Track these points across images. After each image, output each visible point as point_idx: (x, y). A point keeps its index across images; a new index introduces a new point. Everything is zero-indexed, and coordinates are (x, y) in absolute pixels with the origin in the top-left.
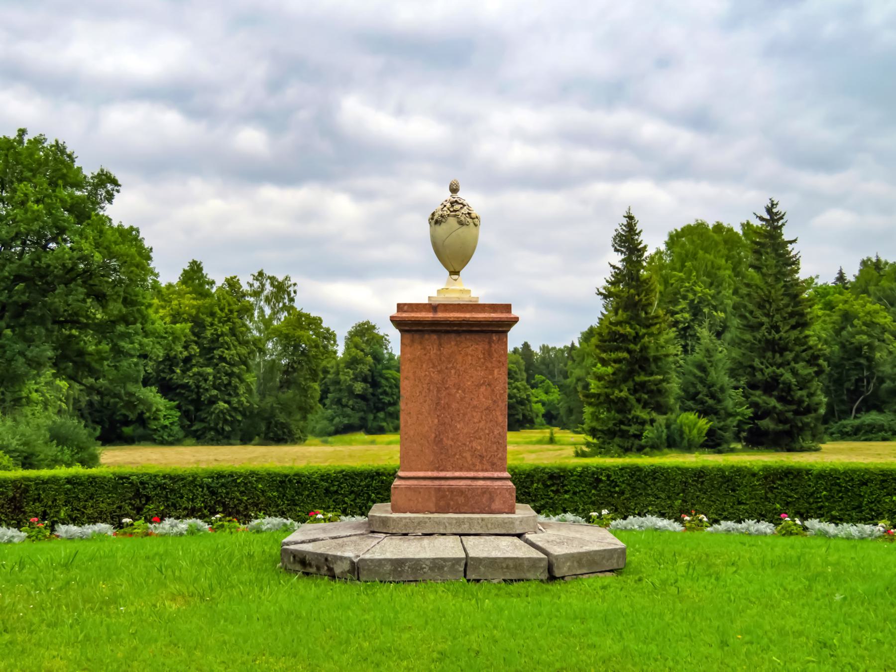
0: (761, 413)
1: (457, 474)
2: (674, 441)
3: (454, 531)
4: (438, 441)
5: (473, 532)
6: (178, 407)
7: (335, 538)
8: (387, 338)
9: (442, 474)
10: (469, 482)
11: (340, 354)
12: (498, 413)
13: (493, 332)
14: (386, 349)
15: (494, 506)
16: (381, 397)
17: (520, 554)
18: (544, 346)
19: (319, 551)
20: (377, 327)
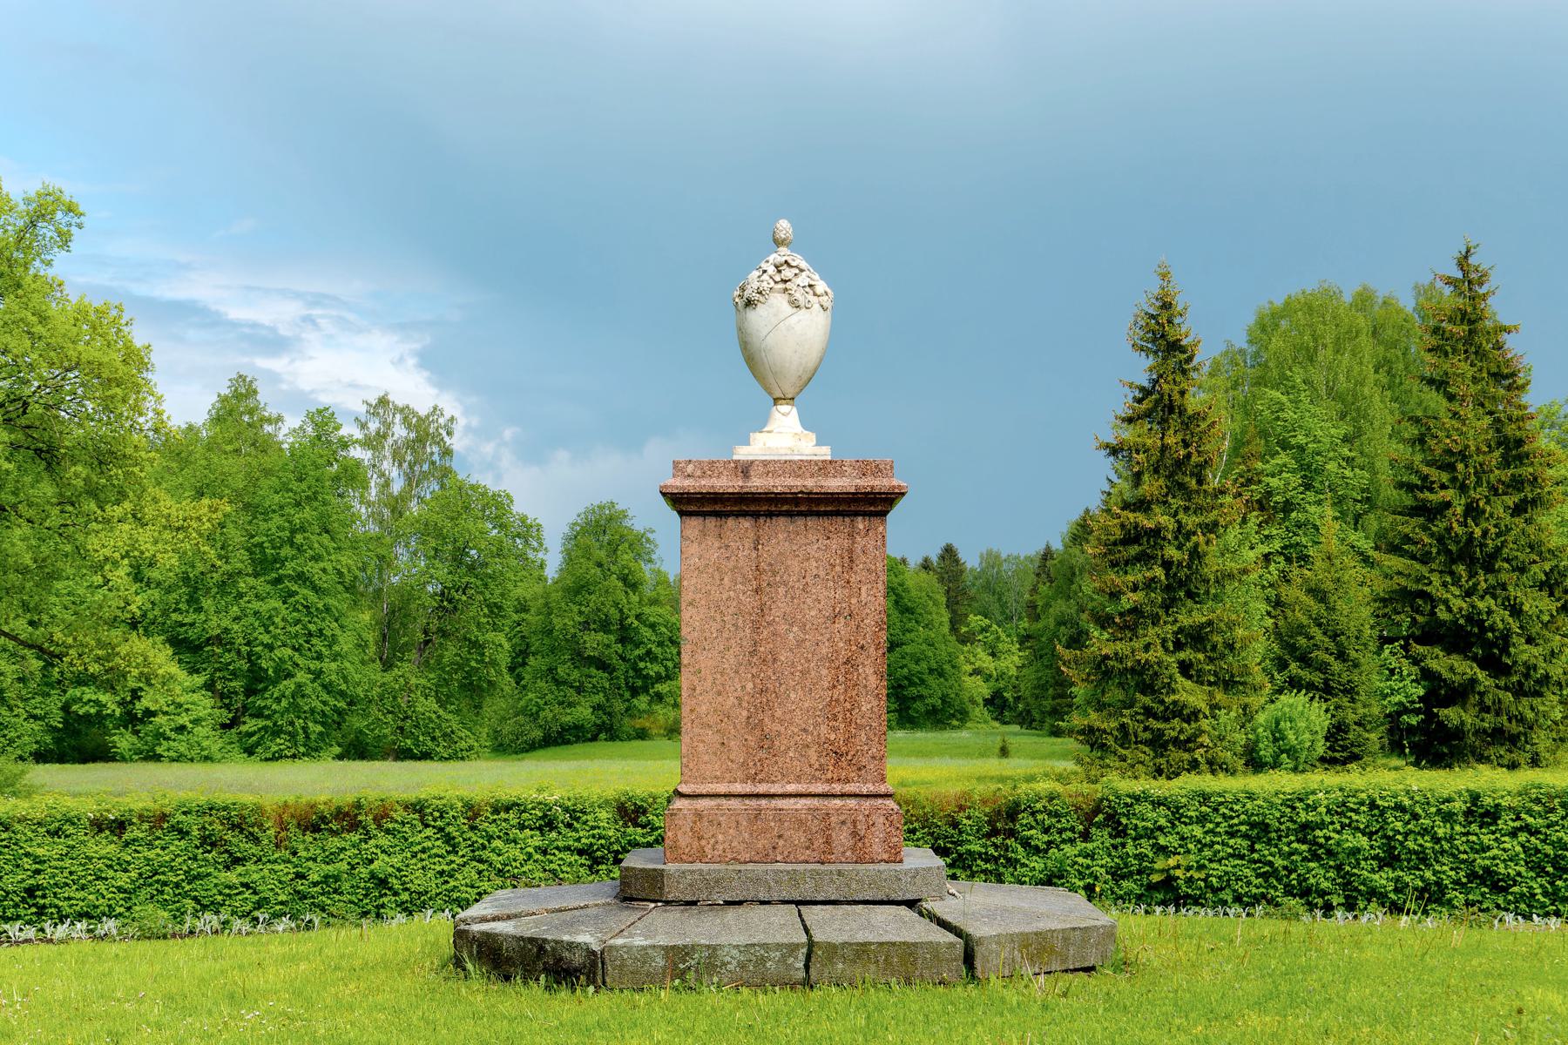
0: (1440, 692)
3: (785, 896)
5: (820, 898)
6: (209, 686)
7: (560, 910)
8: (651, 536)
9: (762, 788)
11: (552, 571)
12: (869, 671)
13: (856, 514)
16: (642, 665)
19: (528, 934)
20: (630, 513)
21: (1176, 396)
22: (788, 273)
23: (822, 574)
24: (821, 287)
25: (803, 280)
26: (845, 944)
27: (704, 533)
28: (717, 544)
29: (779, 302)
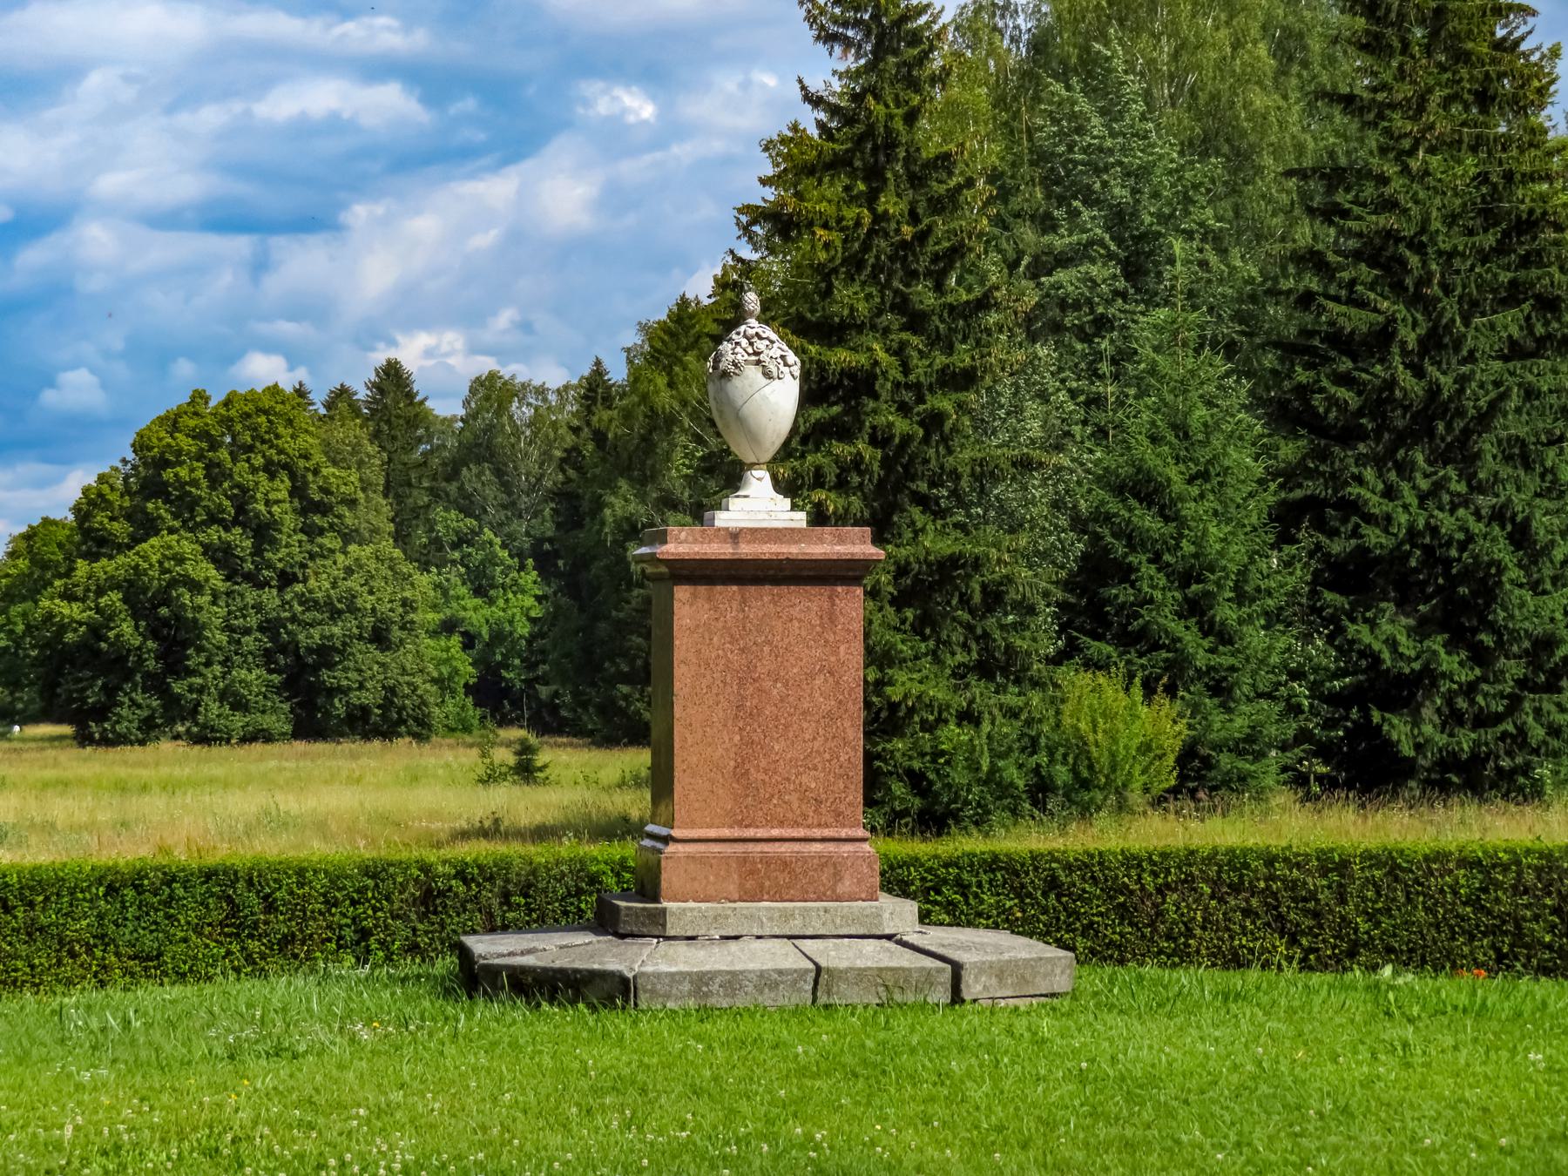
1: (775, 833)
4: (740, 773)
10: (797, 847)
15: (840, 889)
21: (898, 124)
22: (760, 345)
23: (804, 634)
26: (847, 970)
27: (695, 596)
28: (707, 606)
29: (753, 373)
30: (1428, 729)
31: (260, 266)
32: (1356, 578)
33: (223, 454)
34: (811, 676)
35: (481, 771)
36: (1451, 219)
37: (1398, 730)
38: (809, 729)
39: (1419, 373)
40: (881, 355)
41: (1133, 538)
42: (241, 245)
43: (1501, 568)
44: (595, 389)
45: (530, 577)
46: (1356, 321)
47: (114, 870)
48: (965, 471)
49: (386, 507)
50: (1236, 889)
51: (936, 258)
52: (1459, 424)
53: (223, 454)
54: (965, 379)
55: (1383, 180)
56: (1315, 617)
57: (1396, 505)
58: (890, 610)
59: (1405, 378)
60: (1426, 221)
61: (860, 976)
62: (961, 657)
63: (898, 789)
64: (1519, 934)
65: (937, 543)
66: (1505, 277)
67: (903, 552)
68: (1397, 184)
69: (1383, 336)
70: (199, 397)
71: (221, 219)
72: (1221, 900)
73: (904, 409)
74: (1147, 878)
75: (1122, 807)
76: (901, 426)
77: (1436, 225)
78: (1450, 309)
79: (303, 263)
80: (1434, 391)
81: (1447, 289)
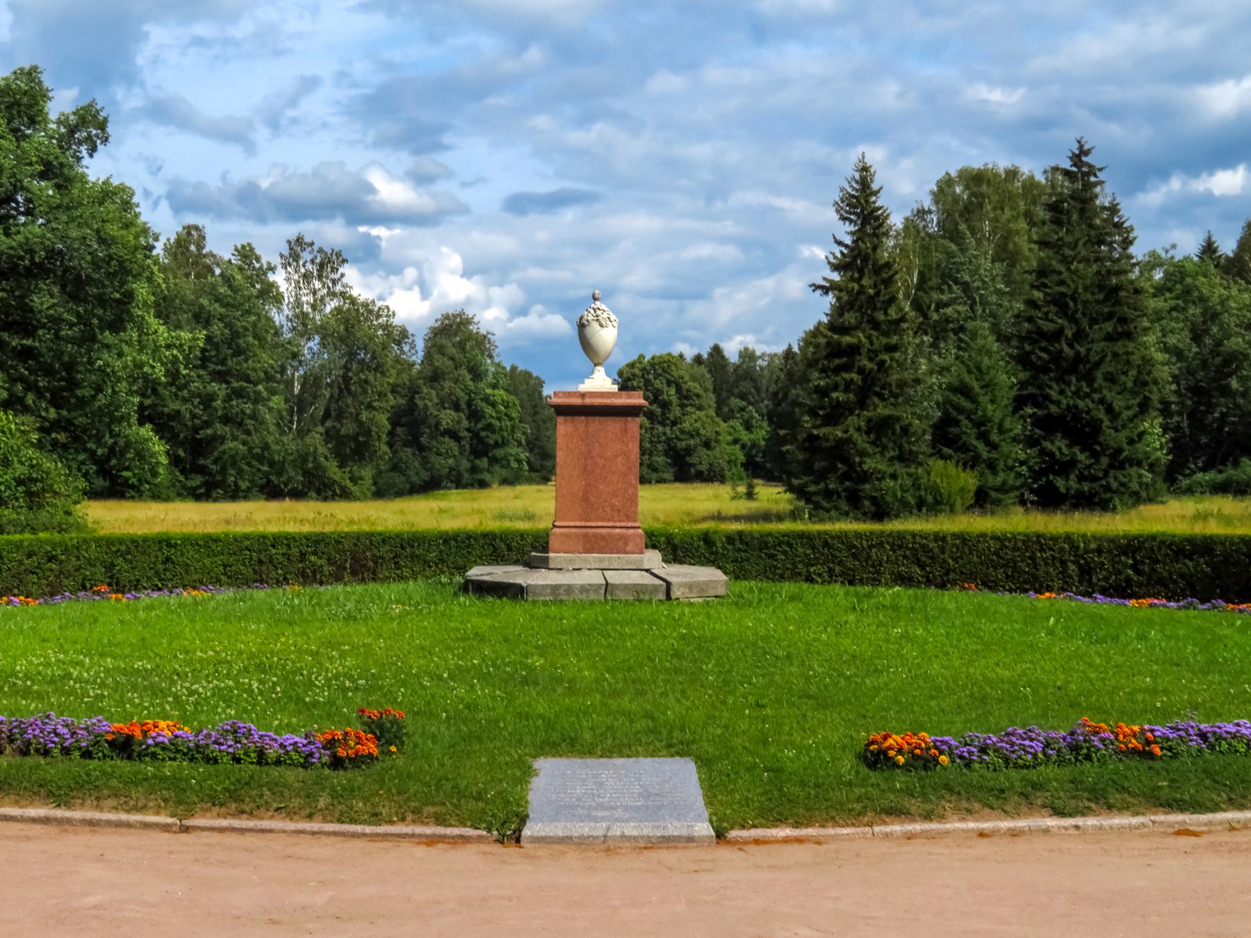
1: (600, 524)
2: (932, 503)
4: (585, 498)
9: (589, 524)
10: (609, 530)
14: (490, 356)
15: (628, 549)
17: (646, 582)
18: (746, 349)
22: (599, 312)
24: (613, 317)
25: (605, 315)
29: (595, 325)
30: (1071, 483)
31: (681, 311)
32: (1048, 425)
33: (651, 377)
34: (617, 456)
35: (732, 494)
36: (1086, 288)
37: (1060, 483)
38: (615, 479)
39: (1071, 346)
40: (863, 339)
41: (960, 410)
42: (673, 304)
43: (1102, 421)
44: (789, 354)
45: (765, 424)
46: (1047, 326)
47: (446, 533)
48: (894, 384)
49: (712, 396)
50: (900, 547)
51: (884, 302)
52: (1088, 366)
53: (651, 377)
54: (892, 349)
55: (1060, 273)
56: (1032, 442)
57: (1061, 397)
58: (865, 436)
59: (1066, 349)
60: (1076, 289)
61: (626, 587)
62: (892, 453)
63: (867, 503)
64: (1015, 568)
65: (883, 410)
66: (1106, 310)
67: (870, 414)
68: (1065, 275)
69: (1059, 333)
70: (642, 357)
71: (666, 294)
72: (894, 551)
73: (871, 360)
74: (864, 543)
75: (952, 511)
76: (869, 365)
77: (1080, 290)
78: (1085, 323)
79: (697, 310)
80: (1078, 354)
81: (1084, 314)
